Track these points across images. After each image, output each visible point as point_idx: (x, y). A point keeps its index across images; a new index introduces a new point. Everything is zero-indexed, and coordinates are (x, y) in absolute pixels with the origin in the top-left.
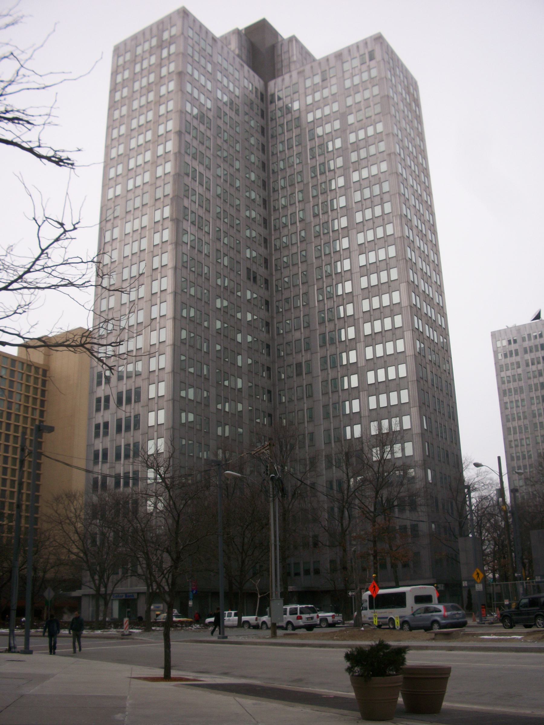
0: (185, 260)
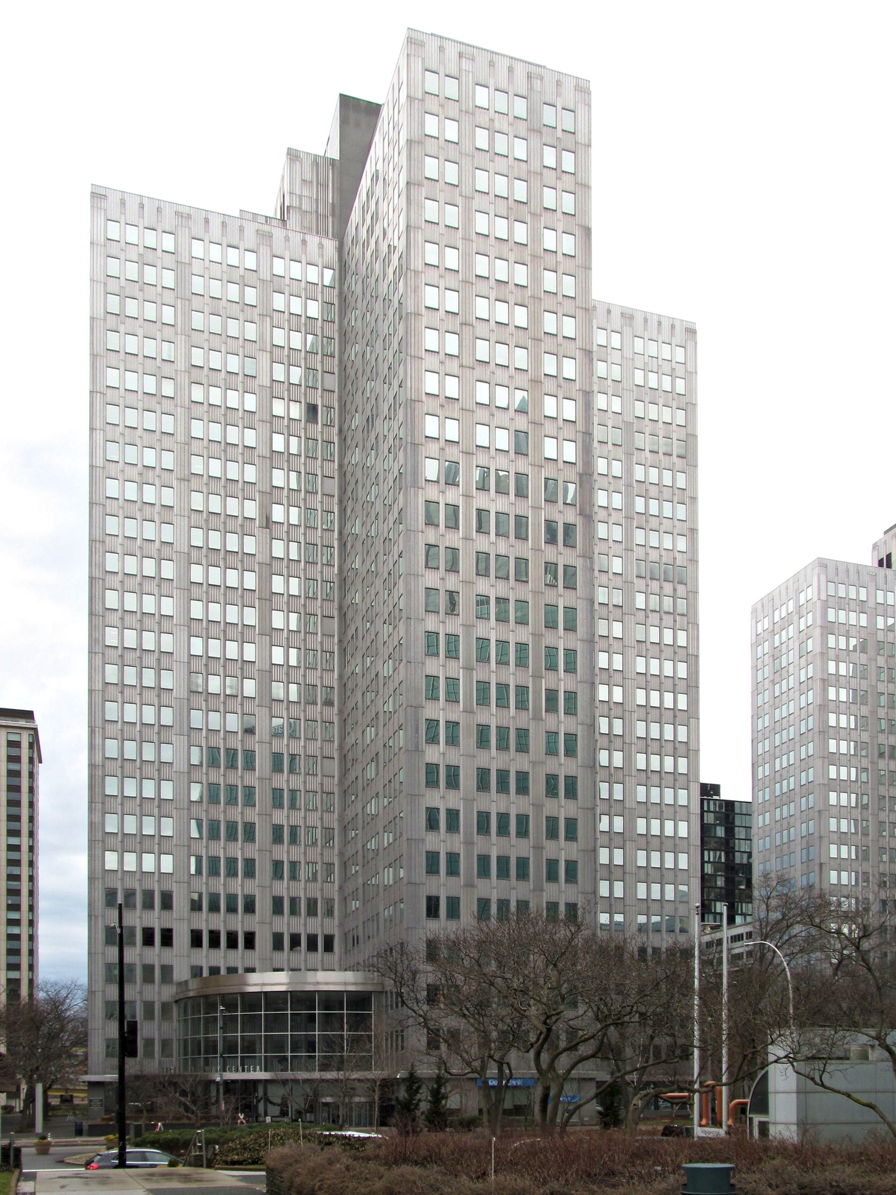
0: (865, 801)
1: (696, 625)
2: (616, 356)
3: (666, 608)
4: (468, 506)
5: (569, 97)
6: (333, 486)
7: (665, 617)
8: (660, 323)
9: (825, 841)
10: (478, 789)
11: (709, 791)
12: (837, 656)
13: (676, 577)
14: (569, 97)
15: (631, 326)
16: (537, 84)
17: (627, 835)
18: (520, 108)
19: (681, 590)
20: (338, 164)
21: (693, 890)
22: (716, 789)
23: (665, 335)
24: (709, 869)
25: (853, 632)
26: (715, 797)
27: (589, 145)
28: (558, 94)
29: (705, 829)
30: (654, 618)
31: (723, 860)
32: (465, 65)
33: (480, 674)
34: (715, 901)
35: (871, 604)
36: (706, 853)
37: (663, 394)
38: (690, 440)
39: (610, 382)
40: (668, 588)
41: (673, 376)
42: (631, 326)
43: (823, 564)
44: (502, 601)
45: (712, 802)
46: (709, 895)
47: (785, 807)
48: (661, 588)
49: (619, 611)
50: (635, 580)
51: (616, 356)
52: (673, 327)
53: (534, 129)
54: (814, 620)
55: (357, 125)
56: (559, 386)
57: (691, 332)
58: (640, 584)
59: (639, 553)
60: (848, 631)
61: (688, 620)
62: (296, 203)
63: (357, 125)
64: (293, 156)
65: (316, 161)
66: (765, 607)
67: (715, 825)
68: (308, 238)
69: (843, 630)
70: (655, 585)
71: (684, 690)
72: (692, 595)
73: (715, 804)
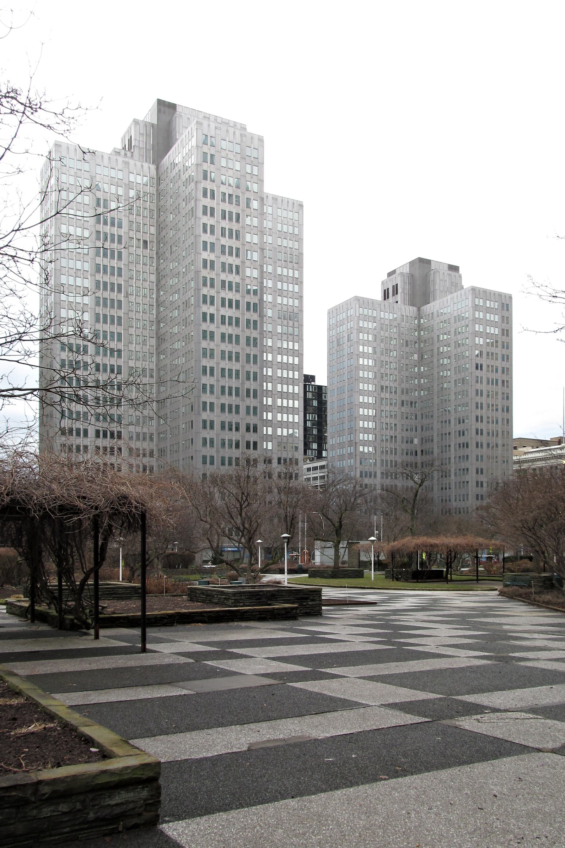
1: (302, 340)
2: (270, 218)
3: (290, 332)
4: (218, 314)
5: (256, 142)
6: (153, 278)
7: (289, 336)
8: (288, 202)
9: (358, 432)
10: (222, 429)
11: (309, 379)
12: (364, 343)
13: (293, 318)
14: (256, 143)
15: (276, 204)
16: (244, 138)
17: (273, 436)
18: (238, 149)
19: (296, 324)
20: (156, 127)
21: (299, 433)
22: (313, 378)
23: (290, 208)
24: (309, 424)
25: (370, 331)
26: (313, 383)
27: (263, 164)
28: (252, 142)
29: (307, 402)
30: (285, 337)
31: (316, 419)
32: (218, 132)
33: (222, 383)
34: (312, 442)
35: (378, 318)
36: (308, 415)
37: (289, 235)
38: (300, 256)
39: (268, 230)
40: (291, 323)
41: (293, 226)
42: (276, 204)
43: (357, 299)
44: (230, 353)
45: (311, 386)
46: (309, 438)
47: (341, 413)
48: (288, 323)
49: (271, 334)
50: (277, 320)
51: (270, 218)
52: (293, 203)
53: (243, 158)
54: (354, 325)
55: (164, 113)
56: (252, 264)
57: (301, 206)
58: (279, 321)
59: (279, 307)
60: (364, 343)
61: (299, 338)
62: (137, 144)
63: (164, 113)
64: (136, 122)
65: (146, 124)
66: (333, 313)
67: (312, 399)
68: (144, 164)
69: (366, 331)
70: (285, 322)
71: (297, 370)
72: (301, 326)
73: (312, 387)
